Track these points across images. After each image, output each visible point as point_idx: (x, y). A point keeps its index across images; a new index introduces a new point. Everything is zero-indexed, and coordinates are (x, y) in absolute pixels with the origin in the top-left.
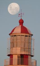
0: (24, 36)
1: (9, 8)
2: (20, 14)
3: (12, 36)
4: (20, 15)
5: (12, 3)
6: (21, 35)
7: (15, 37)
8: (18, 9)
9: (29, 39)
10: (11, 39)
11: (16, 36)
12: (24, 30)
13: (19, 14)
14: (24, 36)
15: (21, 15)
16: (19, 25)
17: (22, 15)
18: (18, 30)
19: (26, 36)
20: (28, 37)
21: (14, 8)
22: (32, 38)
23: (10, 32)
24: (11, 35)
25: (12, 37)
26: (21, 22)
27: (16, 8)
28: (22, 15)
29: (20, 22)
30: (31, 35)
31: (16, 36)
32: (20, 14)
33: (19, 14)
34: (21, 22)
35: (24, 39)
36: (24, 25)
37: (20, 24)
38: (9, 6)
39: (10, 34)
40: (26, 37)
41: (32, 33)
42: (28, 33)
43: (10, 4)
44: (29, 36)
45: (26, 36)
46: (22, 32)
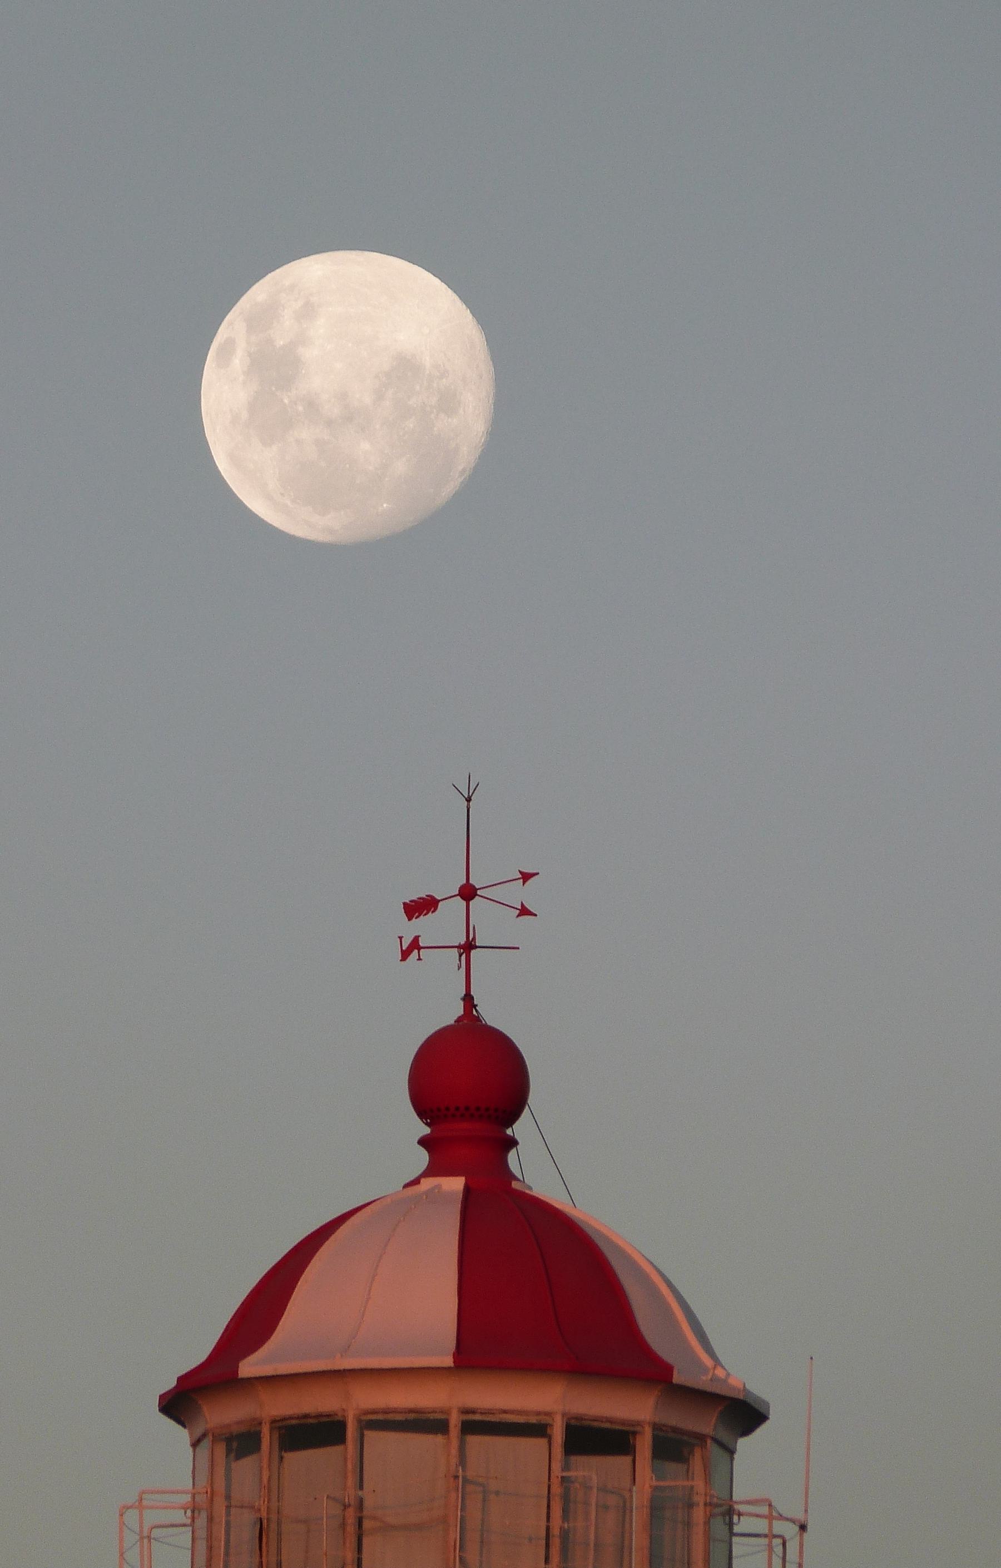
0: (538, 1430)
1: (223, 392)
2: (445, 885)
3: (242, 1442)
4: (444, 925)
5: (313, 271)
6: (477, 1425)
7: (299, 1460)
8: (448, 403)
9: (656, 1509)
10: (206, 1508)
11: (326, 1431)
12: (544, 1294)
13: (419, 907)
14: (538, 1430)
15: (452, 909)
16: (422, 1158)
17: (490, 920)
18: (401, 1300)
19: (587, 1439)
20: (641, 1476)
21: (344, 372)
22: (739, 1493)
23: (196, 1349)
24: (224, 1413)
25: (246, 1468)
26: (470, 1090)
27: (405, 368)
28: (490, 920)
29: (423, 1102)
30: (706, 1424)
31: (326, 1431)
32: (445, 885)
33: (419, 907)
34: (470, 1090)
35: (533, 1522)
36: (547, 1158)
37: (440, 1153)
38: (233, 327)
39: (179, 1403)
40: (593, 1470)
41: (740, 1363)
42: (650, 1371)
43: (259, 293)
44: (671, 1447)
45: (587, 1439)
46: (483, 1342)
